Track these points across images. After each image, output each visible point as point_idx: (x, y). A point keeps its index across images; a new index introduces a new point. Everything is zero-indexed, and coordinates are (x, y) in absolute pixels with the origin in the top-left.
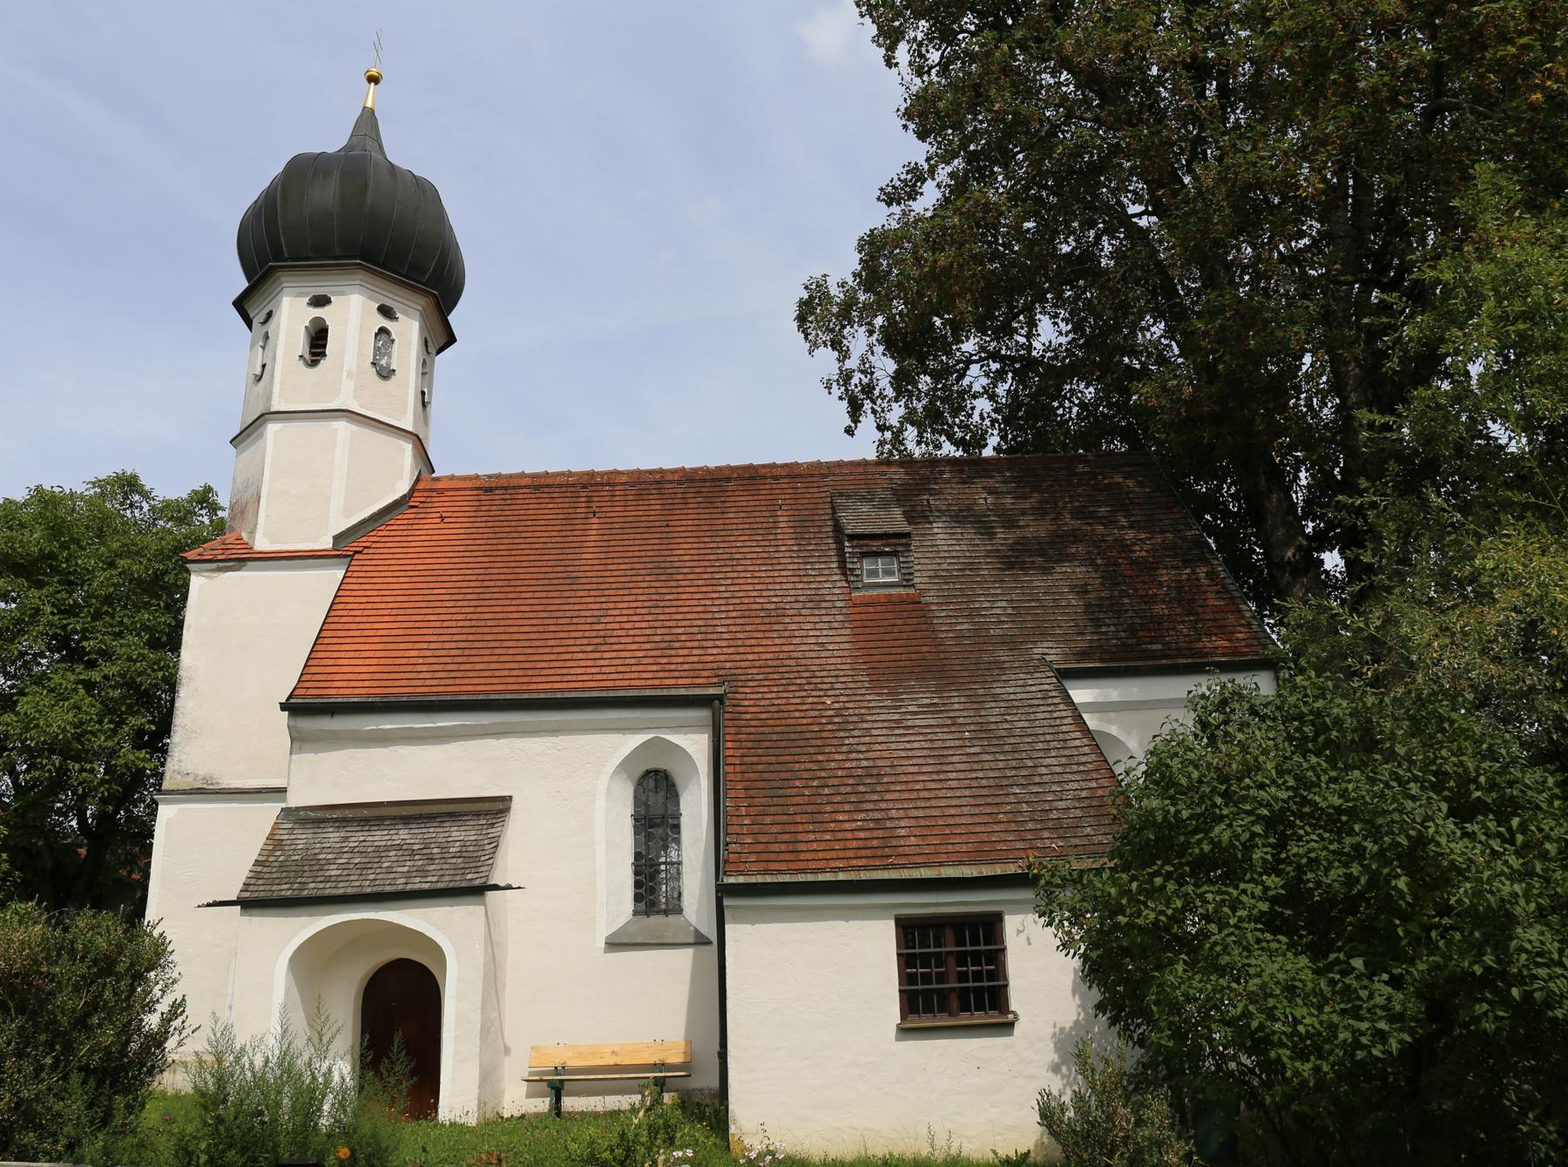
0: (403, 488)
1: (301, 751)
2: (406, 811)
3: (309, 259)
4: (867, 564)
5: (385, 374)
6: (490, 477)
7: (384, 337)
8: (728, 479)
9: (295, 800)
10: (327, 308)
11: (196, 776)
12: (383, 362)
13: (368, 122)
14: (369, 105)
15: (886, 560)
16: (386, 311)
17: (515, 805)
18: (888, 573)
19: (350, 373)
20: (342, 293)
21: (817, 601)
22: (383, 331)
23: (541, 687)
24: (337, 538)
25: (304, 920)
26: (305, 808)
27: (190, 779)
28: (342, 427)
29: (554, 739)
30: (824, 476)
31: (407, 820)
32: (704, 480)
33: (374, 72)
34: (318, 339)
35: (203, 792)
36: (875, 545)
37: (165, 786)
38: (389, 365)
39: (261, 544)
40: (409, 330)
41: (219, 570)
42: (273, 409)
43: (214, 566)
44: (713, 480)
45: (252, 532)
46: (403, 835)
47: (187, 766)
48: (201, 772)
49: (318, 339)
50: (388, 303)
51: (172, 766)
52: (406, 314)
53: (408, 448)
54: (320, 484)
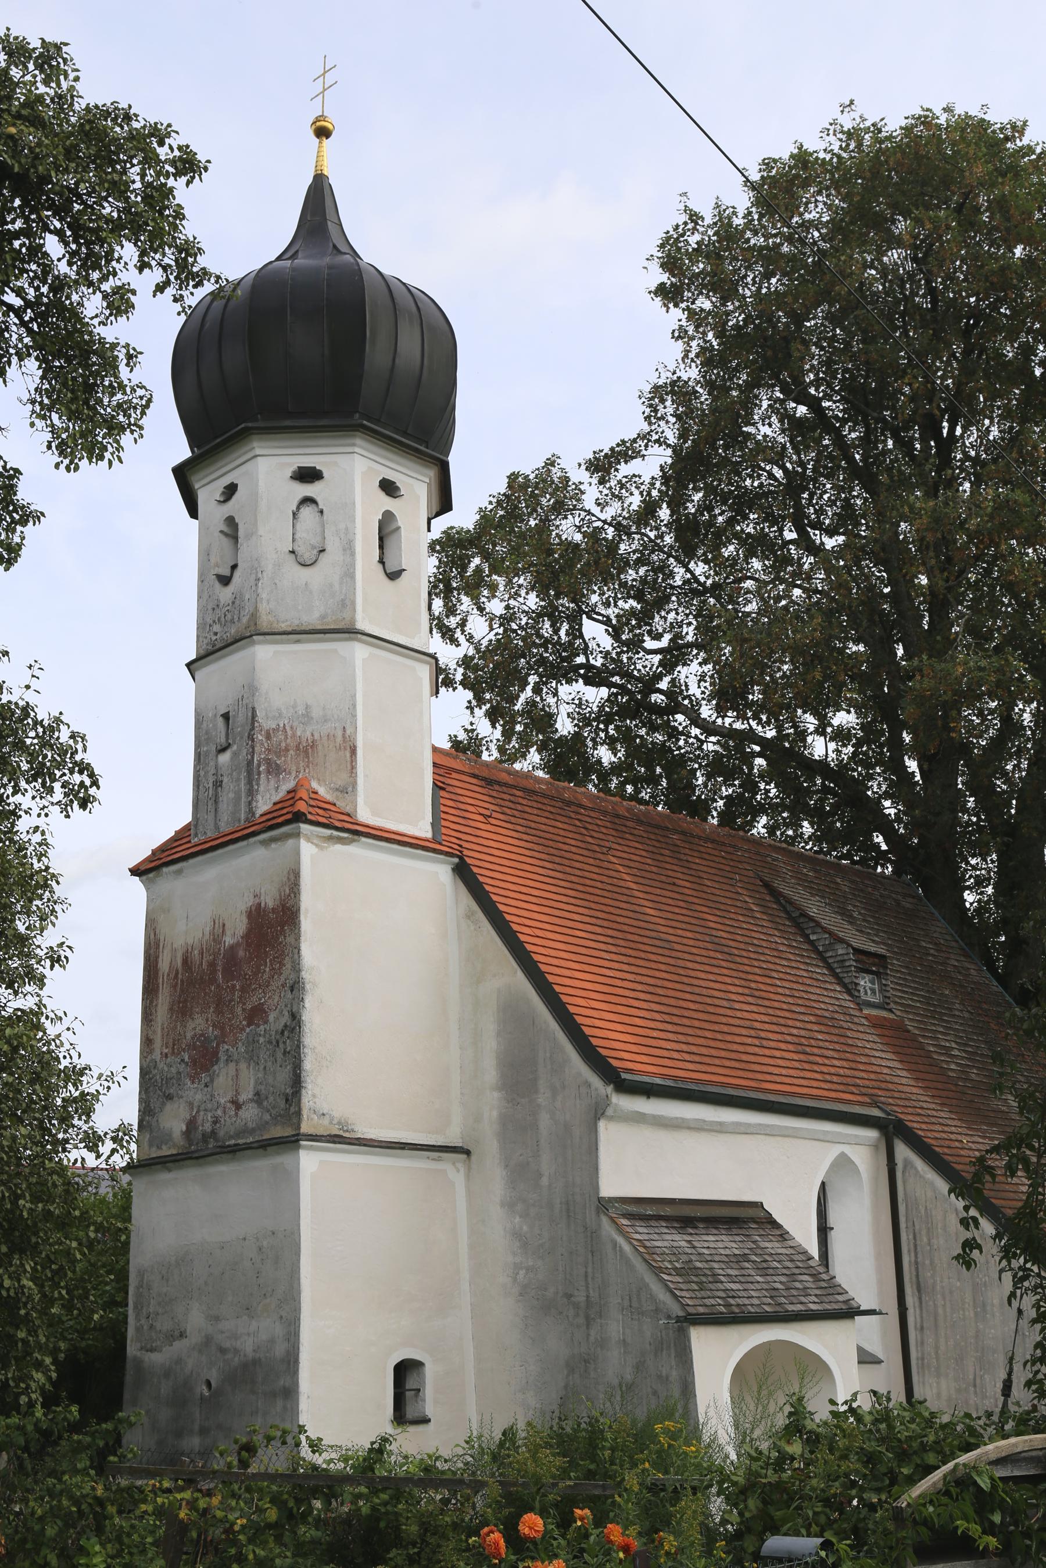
13: (319, 200)
27: (326, 1121)
33: (333, 120)
35: (340, 1139)
39: (365, 815)
41: (330, 838)
45: (348, 789)
50: (392, 476)
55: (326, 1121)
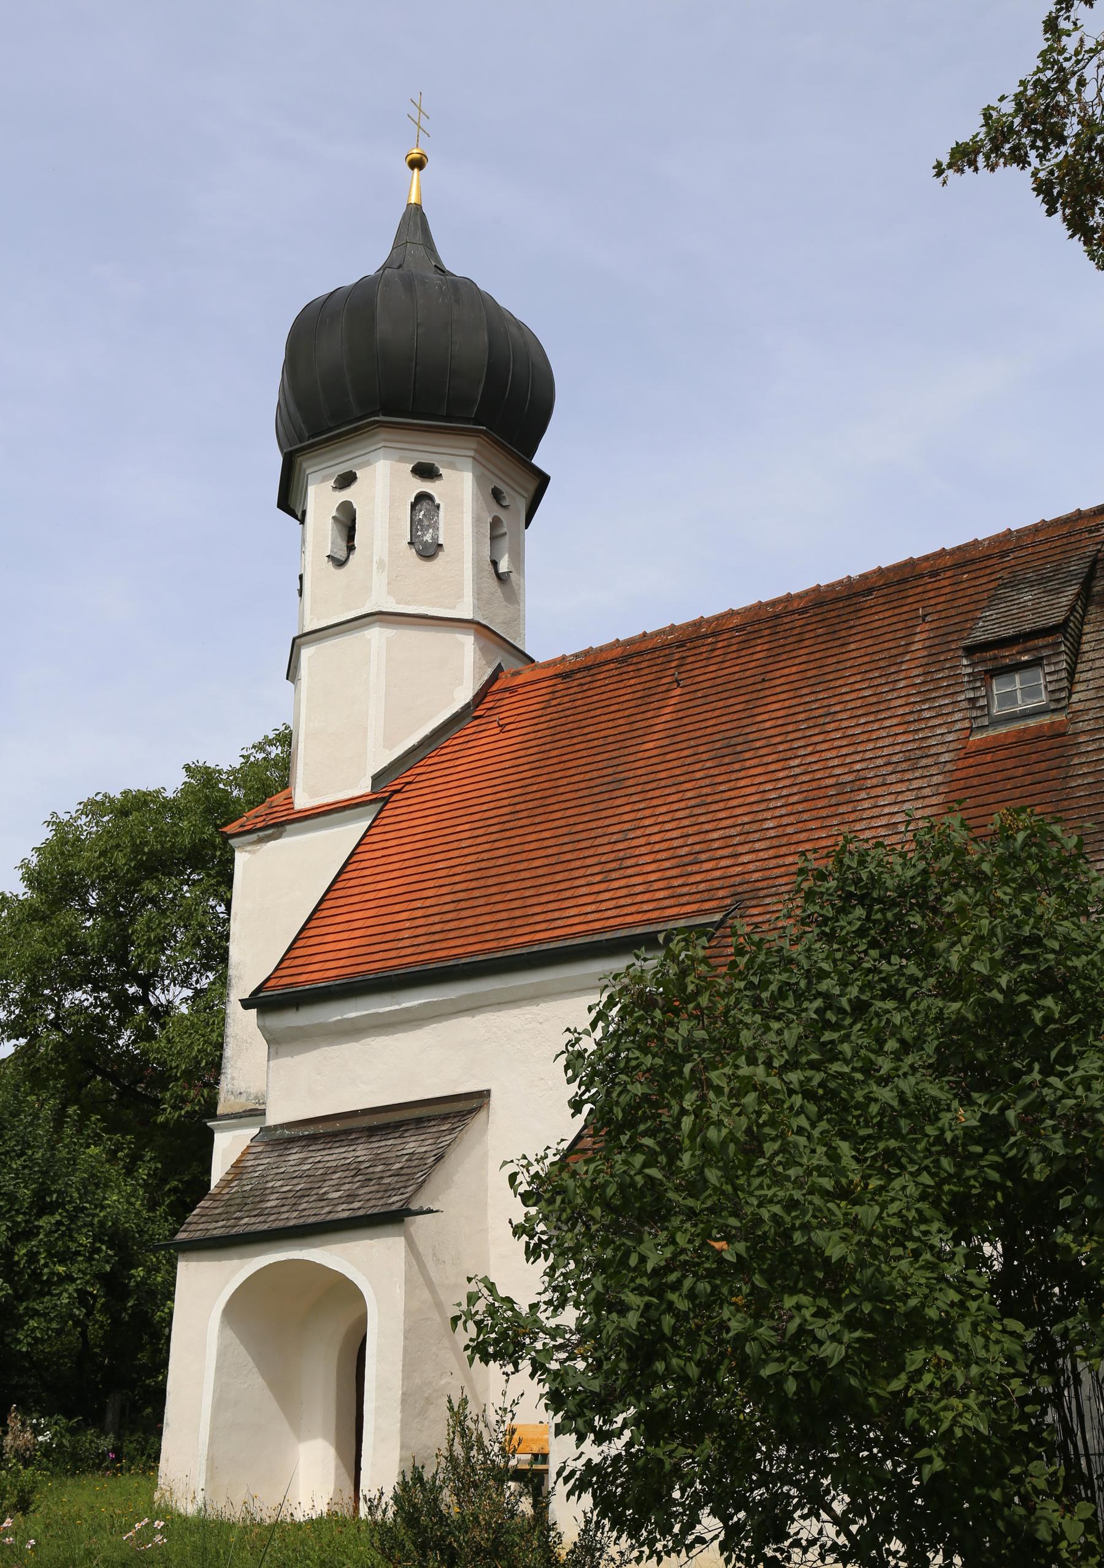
0: (464, 695)
1: (277, 1055)
2: (375, 1121)
3: (330, 429)
4: (998, 687)
5: (429, 552)
6: (576, 656)
7: (425, 505)
8: (870, 591)
9: (273, 1118)
10: (354, 487)
11: (249, 1094)
12: (428, 538)
13: (415, 222)
14: (413, 200)
15: (1028, 674)
16: (426, 472)
17: (495, 1100)
18: (1029, 693)
19: (381, 564)
20: (368, 463)
22: (423, 498)
23: (519, 941)
24: (377, 779)
25: (235, 1263)
28: (376, 634)
29: (534, 1009)
30: (1004, 554)
31: (372, 1132)
33: (415, 153)
36: (1007, 656)
37: (220, 1110)
38: (435, 538)
40: (460, 489)
41: (261, 841)
42: (306, 630)
43: (254, 837)
46: (361, 1152)
47: (241, 1085)
50: (426, 459)
51: (226, 1085)
52: (452, 466)
53: (468, 641)
54: (368, 709)
55: (243, 1099)
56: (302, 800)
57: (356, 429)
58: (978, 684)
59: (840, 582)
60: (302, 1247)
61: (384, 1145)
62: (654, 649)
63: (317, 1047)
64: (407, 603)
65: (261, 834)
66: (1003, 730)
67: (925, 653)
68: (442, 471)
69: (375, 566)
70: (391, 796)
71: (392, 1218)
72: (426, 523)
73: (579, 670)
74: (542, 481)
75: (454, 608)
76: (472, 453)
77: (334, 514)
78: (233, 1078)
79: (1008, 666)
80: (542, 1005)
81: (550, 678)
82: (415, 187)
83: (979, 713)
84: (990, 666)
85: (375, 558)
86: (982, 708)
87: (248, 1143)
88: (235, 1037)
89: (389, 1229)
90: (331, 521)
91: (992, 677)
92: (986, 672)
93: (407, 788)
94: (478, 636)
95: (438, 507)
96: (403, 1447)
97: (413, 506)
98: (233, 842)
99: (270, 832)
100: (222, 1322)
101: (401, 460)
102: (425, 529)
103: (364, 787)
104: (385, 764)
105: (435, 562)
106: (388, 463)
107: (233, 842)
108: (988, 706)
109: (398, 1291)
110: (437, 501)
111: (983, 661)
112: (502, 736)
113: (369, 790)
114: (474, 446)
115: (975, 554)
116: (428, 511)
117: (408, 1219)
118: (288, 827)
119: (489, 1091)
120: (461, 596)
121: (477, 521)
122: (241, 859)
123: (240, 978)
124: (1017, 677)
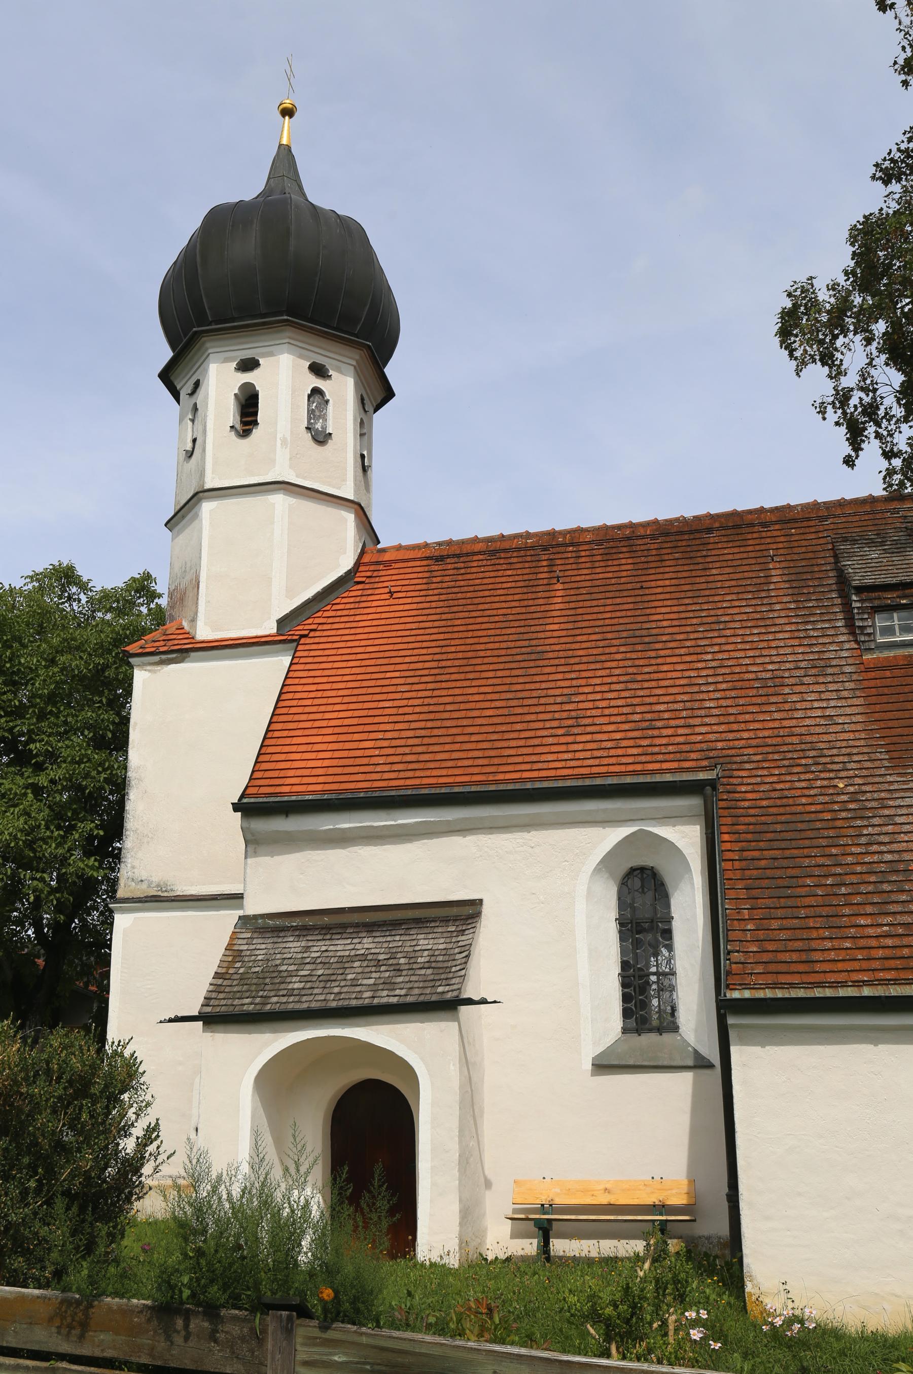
0: (347, 563)
1: (256, 854)
3: (233, 320)
4: (880, 621)
5: (321, 438)
6: (439, 544)
7: (317, 398)
8: (709, 530)
9: (254, 906)
10: (256, 372)
13: (285, 161)
20: (271, 354)
21: (821, 667)
23: (508, 777)
24: (281, 622)
25: (268, 1036)
26: (262, 916)
27: (144, 886)
28: (279, 501)
29: (526, 835)
30: (822, 519)
31: (370, 928)
32: (682, 533)
33: (287, 104)
34: (248, 406)
36: (889, 597)
37: (120, 894)
38: (324, 428)
40: (343, 388)
44: (691, 532)
45: (193, 620)
46: (367, 944)
48: (155, 879)
49: (248, 406)
50: (320, 360)
52: (339, 370)
54: (261, 564)
55: (144, 886)
56: (204, 632)
57: (264, 324)
58: (866, 616)
59: (677, 519)
60: (344, 1026)
61: (397, 940)
62: (518, 549)
63: (300, 849)
64: (305, 478)
65: (164, 657)
66: (892, 654)
67: (787, 586)
68: (331, 372)
69: (279, 442)
70: (300, 639)
71: (450, 1006)
72: (317, 413)
73: (448, 556)
74: (388, 394)
75: (339, 488)
76: (354, 363)
77: (236, 391)
78: (133, 867)
79: (889, 606)
80: (533, 833)
81: (421, 559)
82: (286, 131)
83: (867, 638)
84: (876, 603)
85: (279, 436)
86: (869, 634)
87: (232, 929)
88: (135, 831)
89: (442, 1014)
90: (233, 397)
91: (875, 612)
92: (872, 608)
93: (312, 634)
94: (357, 516)
95: (327, 402)
96: (460, 1201)
97: (309, 396)
98: (132, 660)
99: (174, 656)
100: (253, 1092)
101: (301, 356)
102: (317, 418)
103: (270, 628)
104: (287, 611)
105: (325, 447)
106: (291, 357)
107: (132, 660)
108: (874, 634)
109: (452, 1067)
110: (328, 397)
111: (870, 600)
112: (392, 601)
113: (274, 631)
114: (357, 357)
115: (789, 516)
116: (319, 404)
117: (463, 1009)
118: (193, 654)
119: (481, 901)
120: (345, 480)
121: (355, 420)
122: (141, 677)
123: (140, 780)
124: (895, 615)
